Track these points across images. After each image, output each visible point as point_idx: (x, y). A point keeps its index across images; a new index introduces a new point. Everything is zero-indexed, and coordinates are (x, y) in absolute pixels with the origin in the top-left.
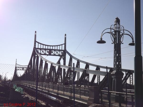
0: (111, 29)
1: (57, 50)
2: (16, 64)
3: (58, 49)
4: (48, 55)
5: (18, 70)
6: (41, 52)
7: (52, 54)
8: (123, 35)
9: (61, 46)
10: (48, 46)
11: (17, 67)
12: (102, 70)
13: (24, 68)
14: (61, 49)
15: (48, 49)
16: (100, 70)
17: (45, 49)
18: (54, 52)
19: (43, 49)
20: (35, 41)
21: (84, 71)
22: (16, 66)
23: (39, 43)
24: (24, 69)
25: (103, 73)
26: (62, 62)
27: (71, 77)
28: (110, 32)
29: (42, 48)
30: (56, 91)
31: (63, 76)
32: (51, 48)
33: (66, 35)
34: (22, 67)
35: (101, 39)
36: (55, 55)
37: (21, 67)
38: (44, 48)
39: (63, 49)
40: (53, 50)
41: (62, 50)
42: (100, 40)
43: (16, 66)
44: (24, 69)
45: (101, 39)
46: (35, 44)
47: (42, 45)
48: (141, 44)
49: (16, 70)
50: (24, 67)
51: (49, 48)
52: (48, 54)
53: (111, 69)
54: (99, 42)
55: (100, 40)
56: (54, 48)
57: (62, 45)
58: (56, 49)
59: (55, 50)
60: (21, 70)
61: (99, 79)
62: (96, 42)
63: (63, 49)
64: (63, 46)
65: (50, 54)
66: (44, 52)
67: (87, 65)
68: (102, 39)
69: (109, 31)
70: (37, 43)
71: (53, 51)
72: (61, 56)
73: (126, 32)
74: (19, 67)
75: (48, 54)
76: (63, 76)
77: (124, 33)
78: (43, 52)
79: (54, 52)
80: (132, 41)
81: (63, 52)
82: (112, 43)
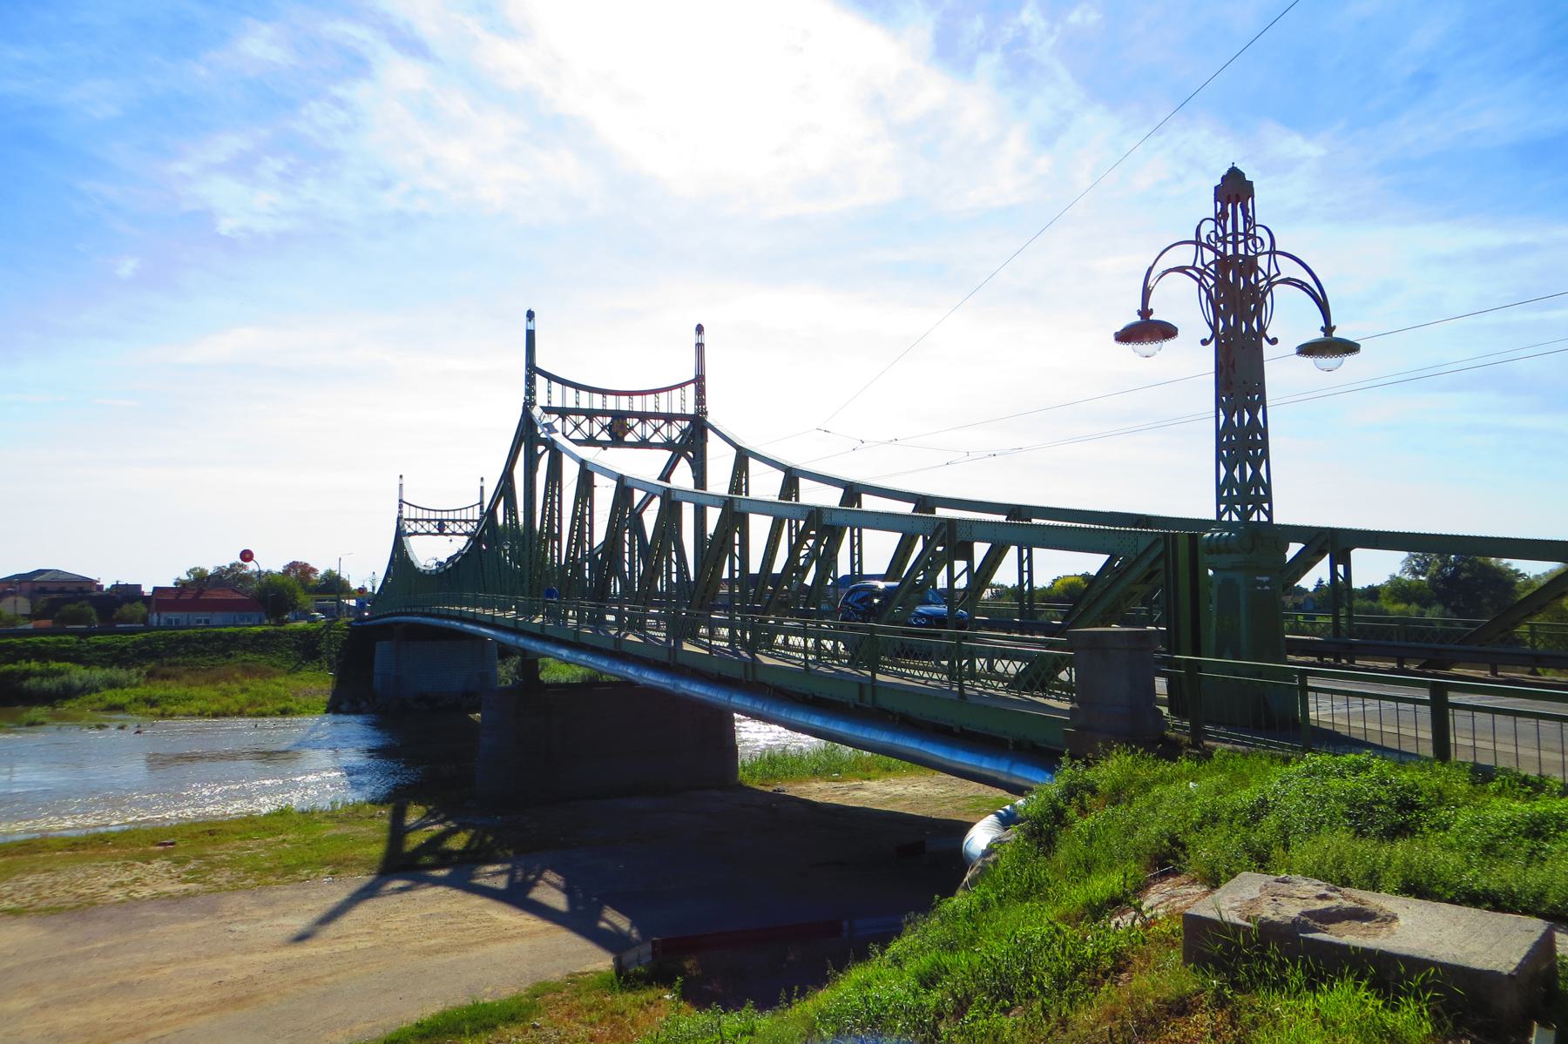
0: (1198, 243)
1: (657, 416)
2: (401, 501)
3: (663, 409)
4: (604, 445)
5: (416, 533)
6: (457, 527)
7: (629, 438)
8: (1271, 285)
10: (604, 392)
11: (409, 520)
12: (870, 503)
13: (448, 520)
14: (470, 518)
15: (604, 413)
16: (860, 506)
17: (429, 521)
18: (638, 430)
19: (577, 411)
20: (532, 370)
21: (726, 502)
22: (401, 512)
23: (550, 377)
24: (447, 531)
25: (883, 521)
26: (683, 477)
28: (1193, 267)
29: (571, 404)
30: (737, 701)
34: (435, 520)
35: (1145, 312)
36: (644, 443)
37: (432, 517)
38: (584, 405)
39: (691, 410)
40: (632, 414)
41: (683, 417)
42: (1138, 319)
43: (401, 512)
44: (447, 531)
45: (1145, 312)
46: (530, 382)
47: (571, 391)
48: (1265, 363)
49: (400, 535)
50: (445, 517)
52: (605, 436)
53: (919, 500)
54: (1127, 336)
55: (1138, 319)
56: (451, 517)
58: (457, 517)
59: (454, 521)
60: (429, 533)
62: (1113, 338)
63: (691, 410)
64: (691, 389)
65: (617, 440)
67: (792, 478)
68: (1151, 312)
69: (1186, 256)
70: (541, 381)
72: (677, 450)
73: (1289, 269)
74: (416, 521)
75: (605, 436)
77: (1279, 274)
79: (452, 527)
80: (1322, 329)
81: (687, 423)
82: (1204, 342)
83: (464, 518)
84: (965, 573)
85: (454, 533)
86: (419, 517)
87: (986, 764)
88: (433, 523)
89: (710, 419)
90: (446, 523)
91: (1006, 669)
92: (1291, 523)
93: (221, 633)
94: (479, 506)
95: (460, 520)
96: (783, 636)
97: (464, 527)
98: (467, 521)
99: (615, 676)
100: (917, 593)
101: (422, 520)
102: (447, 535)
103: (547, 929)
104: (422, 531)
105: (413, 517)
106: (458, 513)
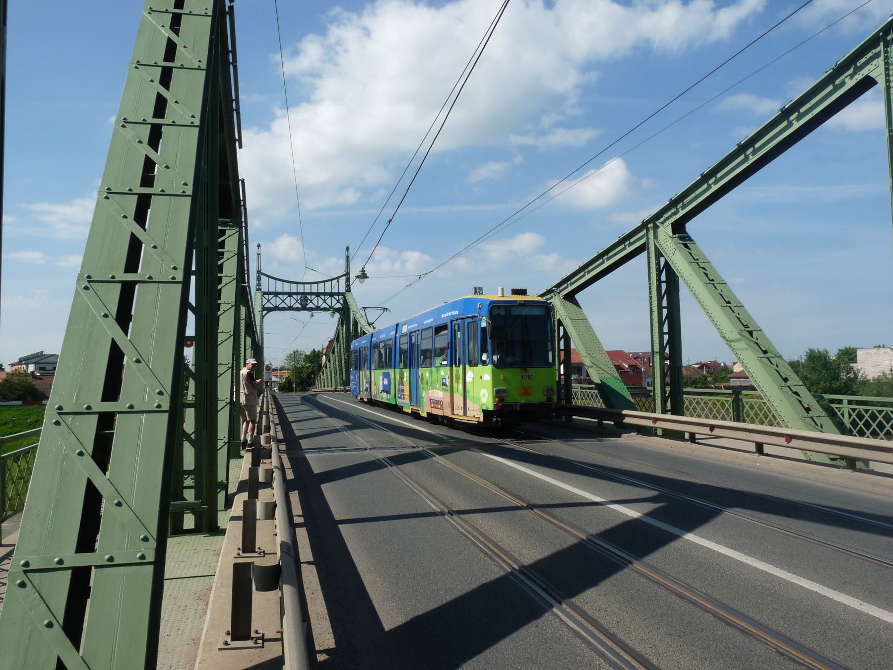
4: (297, 309)
6: (321, 302)
9: (335, 282)
14: (335, 290)
17: (290, 294)
24: (310, 305)
27: (261, 418)
31: (424, 497)
32: (307, 289)
33: (348, 249)
51: (301, 289)
56: (314, 290)
57: (338, 278)
58: (321, 290)
59: (318, 295)
60: (290, 308)
61: (189, 425)
64: (343, 280)
66: (328, 301)
71: (313, 297)
74: (276, 294)
76: (424, 497)
78: (325, 301)
79: (315, 301)
83: (328, 290)
84: (218, 448)
85: (318, 308)
86: (279, 290)
87: (781, 650)
88: (295, 297)
89: (804, 386)
90: (309, 297)
91: (646, 400)
92: (838, 113)
93: (264, 426)
94: (344, 278)
95: (325, 294)
96: (318, 655)
97: (287, 301)
98: (331, 295)
99: (473, 451)
100: (290, 549)
101: (283, 293)
102: (311, 309)
103: (616, 378)
104: (283, 305)
105: (272, 290)
106: (321, 285)
